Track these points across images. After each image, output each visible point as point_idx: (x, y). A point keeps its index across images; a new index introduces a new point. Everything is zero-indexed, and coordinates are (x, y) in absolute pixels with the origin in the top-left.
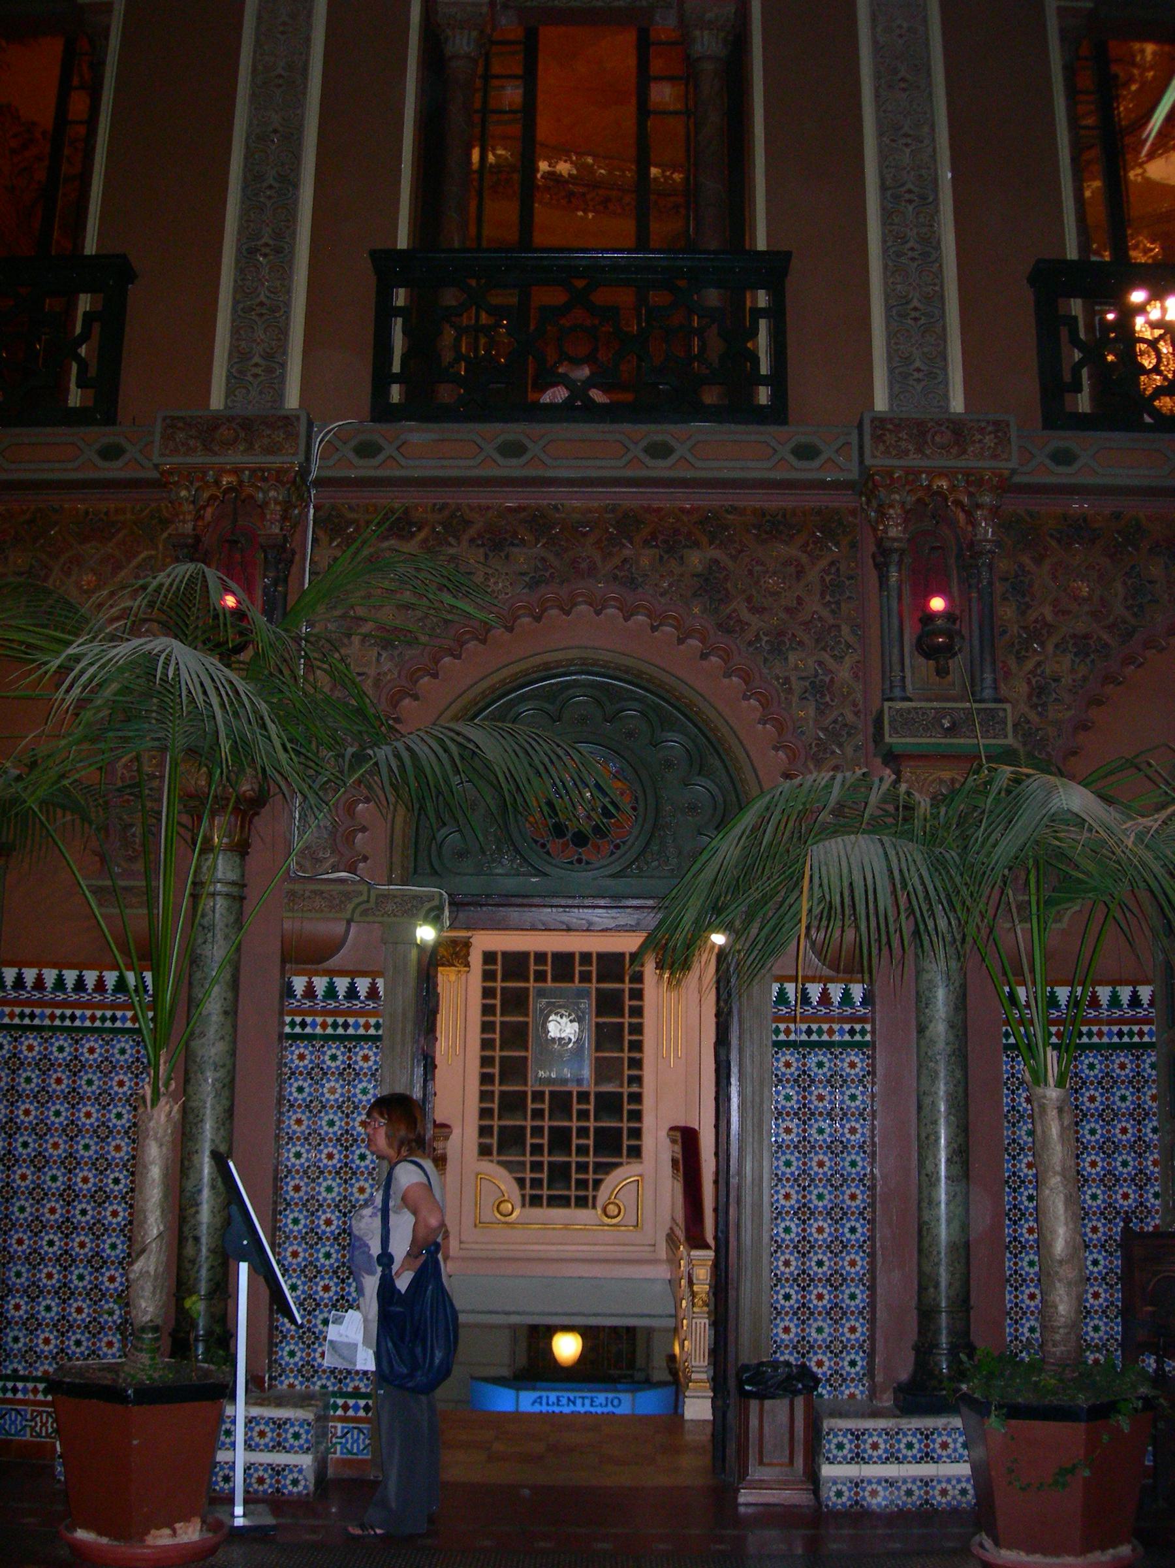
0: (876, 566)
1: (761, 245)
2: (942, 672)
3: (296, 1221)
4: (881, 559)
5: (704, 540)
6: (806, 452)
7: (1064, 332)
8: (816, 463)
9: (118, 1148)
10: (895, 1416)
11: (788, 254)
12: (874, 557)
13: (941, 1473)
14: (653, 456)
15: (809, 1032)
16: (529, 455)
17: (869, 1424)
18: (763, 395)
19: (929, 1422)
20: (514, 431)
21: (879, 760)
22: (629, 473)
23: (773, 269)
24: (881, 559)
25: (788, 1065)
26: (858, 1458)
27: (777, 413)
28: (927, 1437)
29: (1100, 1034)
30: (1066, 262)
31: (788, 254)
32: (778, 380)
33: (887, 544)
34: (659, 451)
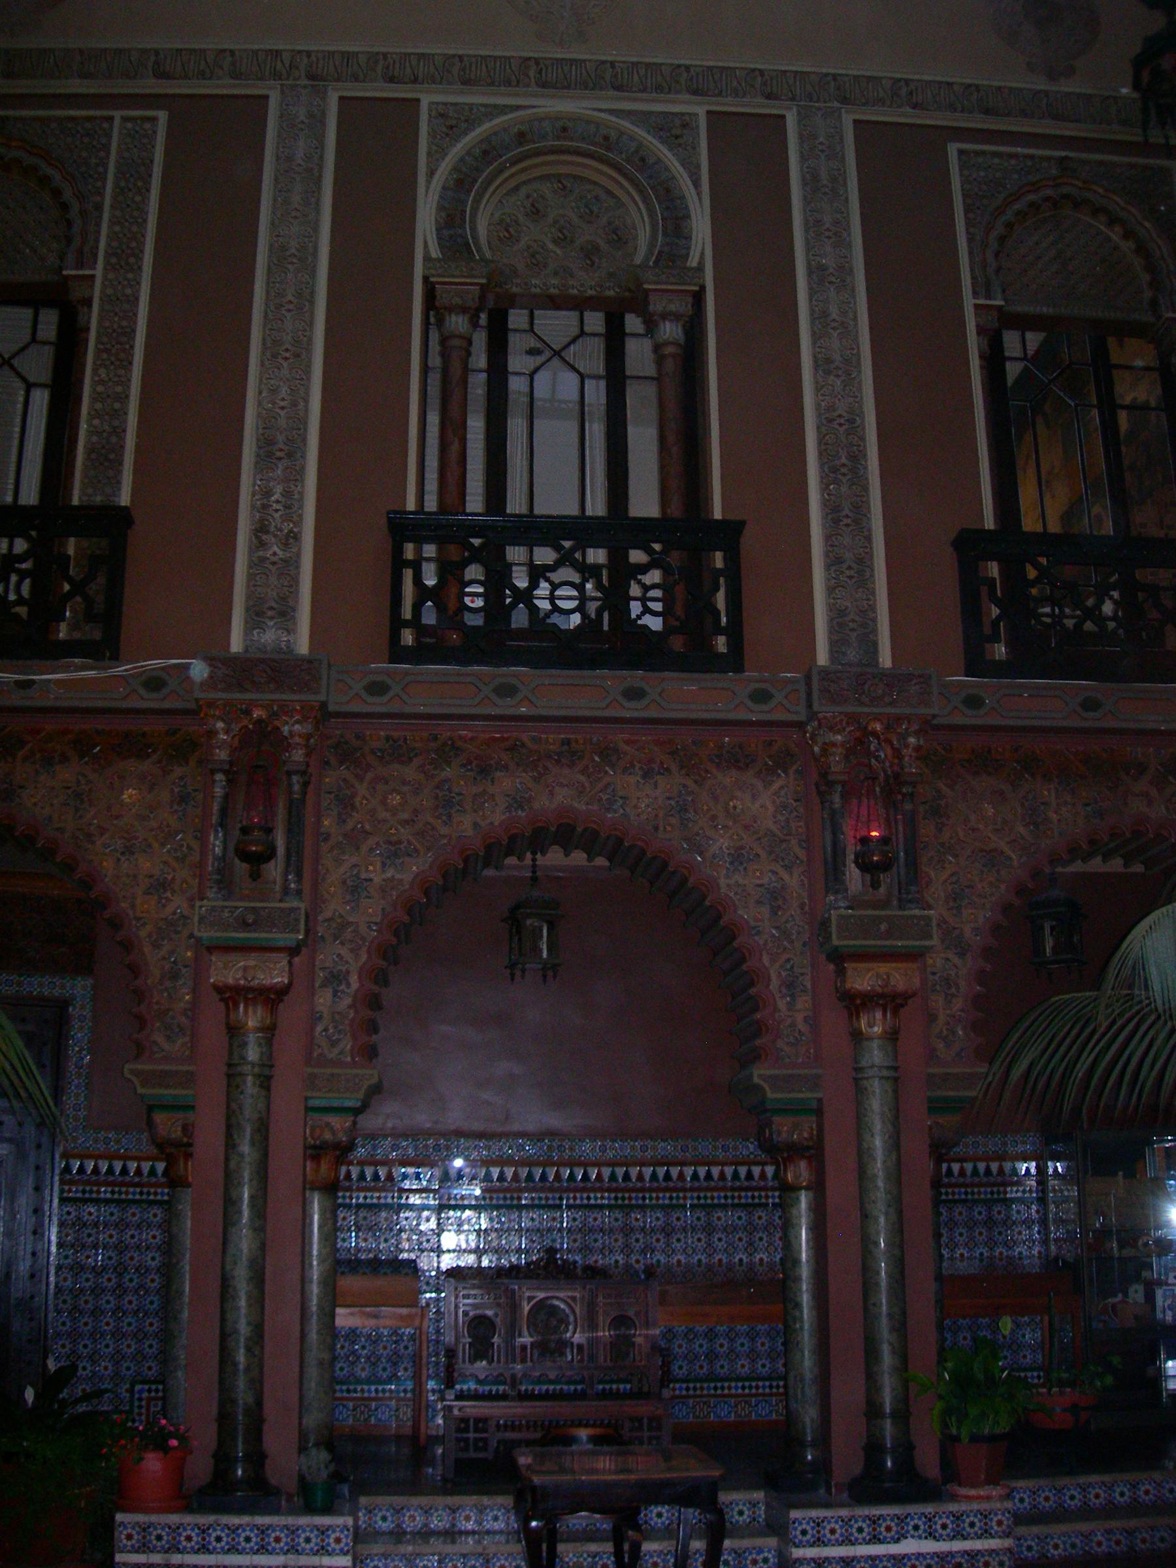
0: (819, 793)
1: (718, 515)
2: (875, 885)
3: (151, 1346)
4: (823, 788)
5: (674, 768)
6: (761, 696)
7: (984, 590)
8: (385, 699)
9: (153, 1281)
10: (849, 1505)
11: (742, 523)
12: (817, 785)
13: (858, 1554)
14: (372, 694)
15: (84, 1192)
16: (391, 694)
17: (828, 1513)
18: (721, 643)
19: (876, 1511)
20: (636, 677)
21: (823, 957)
22: (608, 713)
23: (729, 534)
24: (823, 788)
25: (155, 1215)
26: (819, 1542)
27: (735, 661)
28: (818, 1525)
29: (127, 1193)
30: (983, 531)
31: (742, 523)
32: (735, 632)
33: (830, 778)
34: (634, 694)
